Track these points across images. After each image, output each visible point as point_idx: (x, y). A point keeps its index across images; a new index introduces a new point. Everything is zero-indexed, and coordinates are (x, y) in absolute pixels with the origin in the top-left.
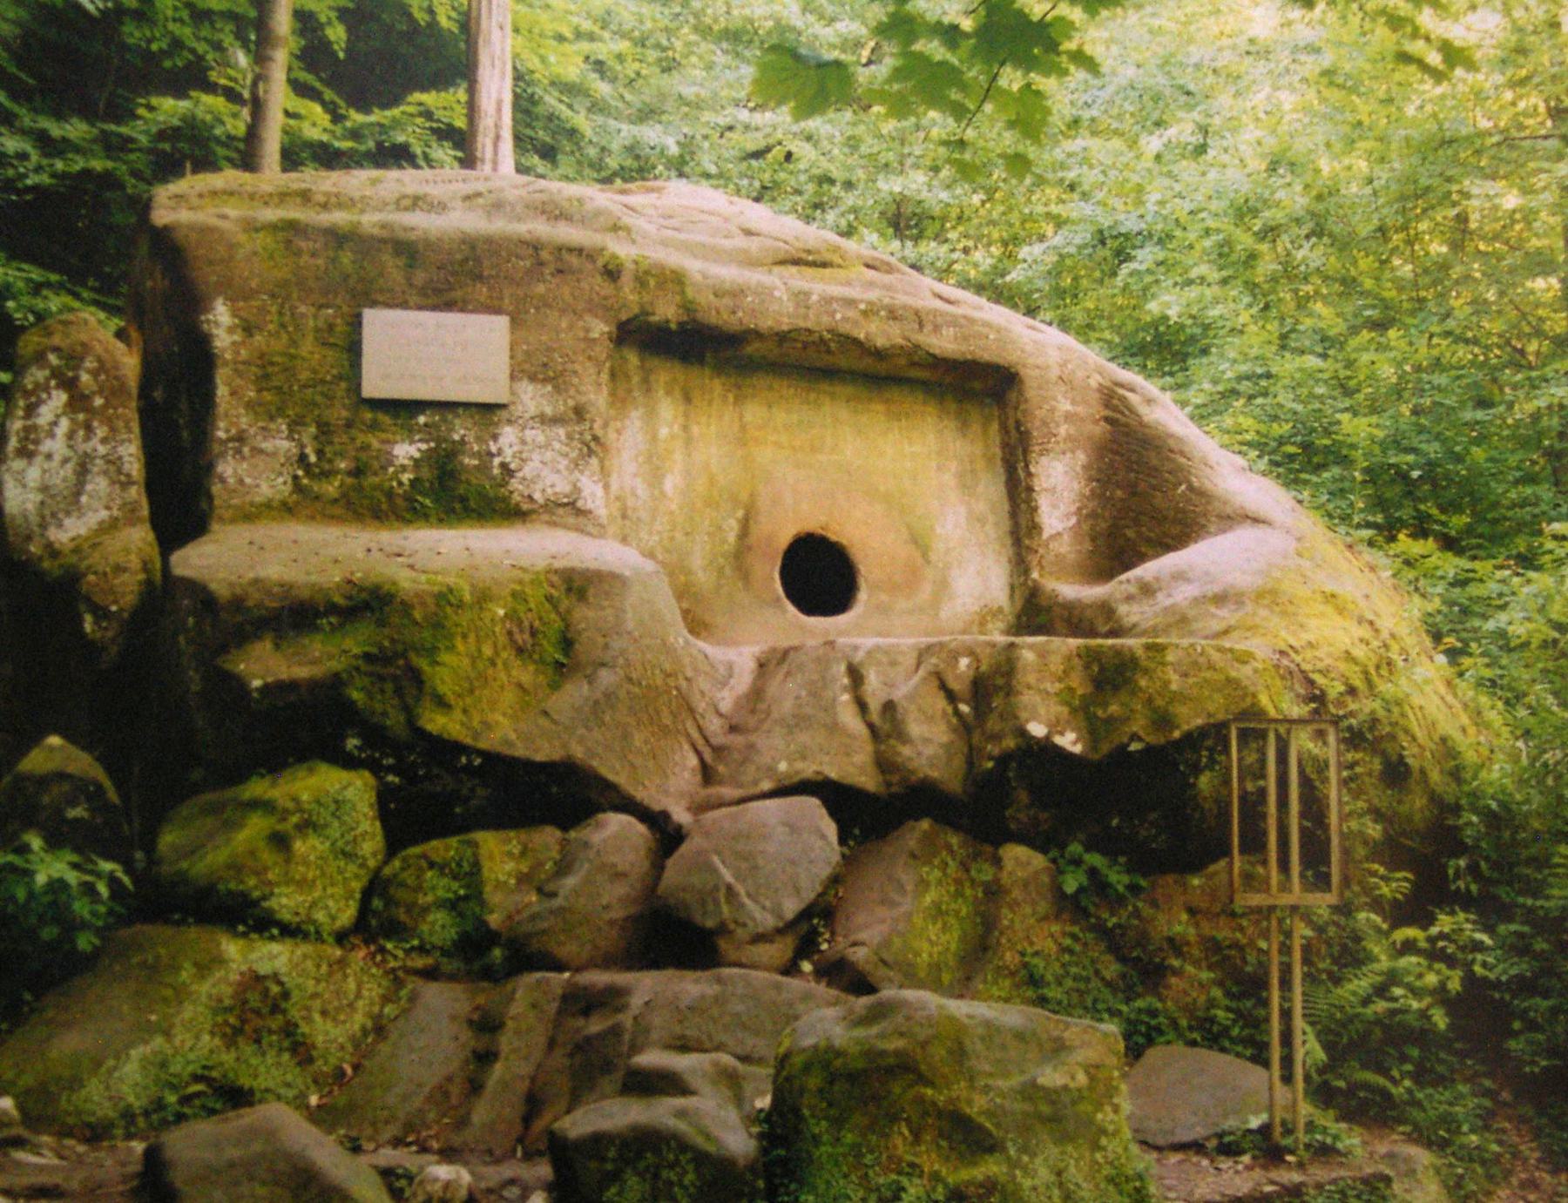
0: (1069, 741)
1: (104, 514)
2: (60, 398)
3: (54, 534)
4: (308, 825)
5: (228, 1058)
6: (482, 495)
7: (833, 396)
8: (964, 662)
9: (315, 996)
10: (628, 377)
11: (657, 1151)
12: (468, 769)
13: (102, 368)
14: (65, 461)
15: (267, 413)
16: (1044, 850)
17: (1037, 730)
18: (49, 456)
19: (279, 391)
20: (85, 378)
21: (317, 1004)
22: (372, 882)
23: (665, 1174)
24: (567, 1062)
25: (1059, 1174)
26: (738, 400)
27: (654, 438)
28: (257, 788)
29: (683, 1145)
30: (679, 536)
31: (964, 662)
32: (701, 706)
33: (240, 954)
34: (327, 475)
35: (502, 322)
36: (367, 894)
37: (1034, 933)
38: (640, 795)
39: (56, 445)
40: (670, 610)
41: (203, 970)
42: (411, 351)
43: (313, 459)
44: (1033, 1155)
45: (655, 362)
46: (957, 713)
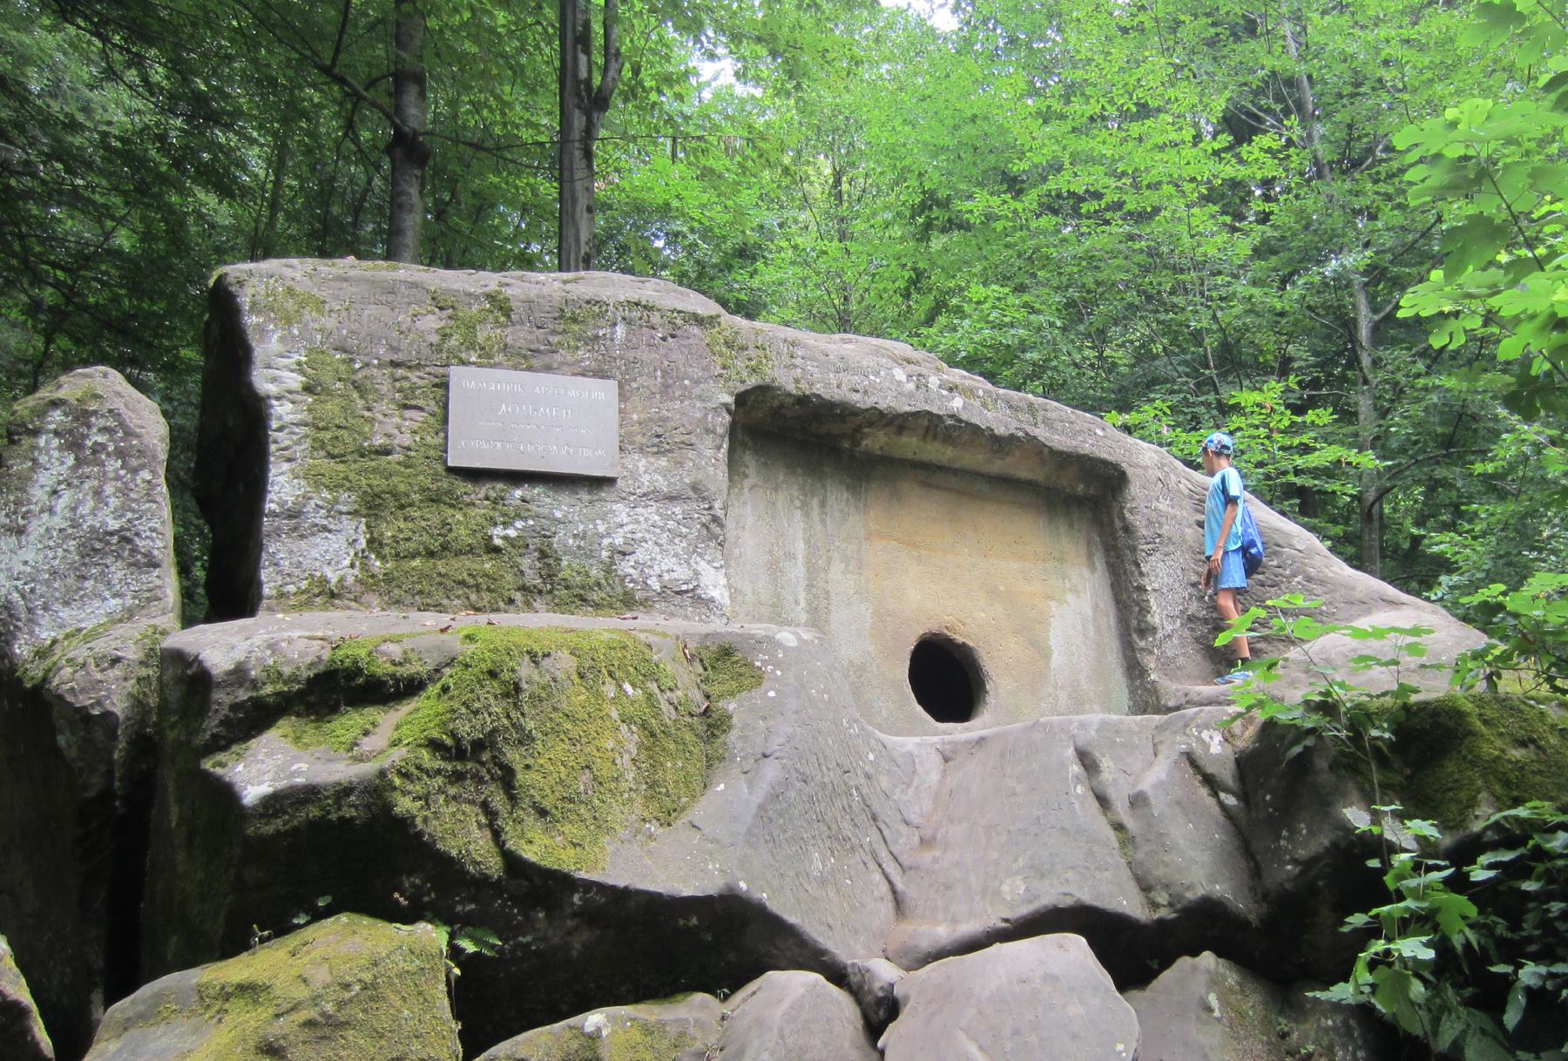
32: (886, 813)
35: (612, 386)
43: (355, 395)
46: (1221, 804)
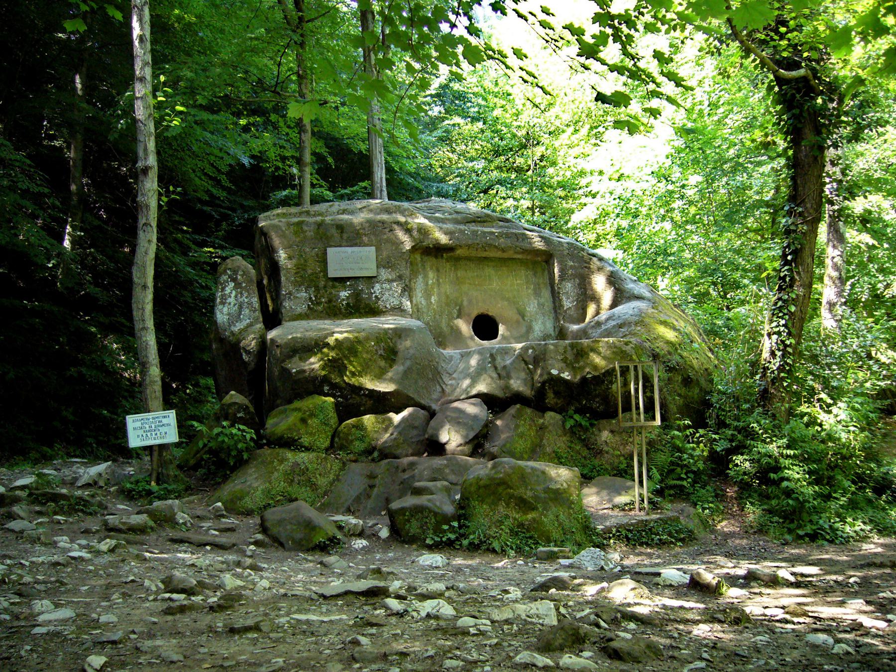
0: (566, 375)
1: (248, 321)
2: (232, 284)
3: (233, 328)
4: (313, 415)
5: (289, 489)
6: (367, 305)
7: (488, 266)
8: (530, 351)
9: (317, 469)
10: (417, 265)
11: (422, 513)
12: (364, 395)
13: (244, 273)
14: (235, 305)
15: (297, 284)
16: (560, 413)
17: (554, 372)
18: (230, 304)
19: (306, 279)
20: (239, 277)
21: (318, 472)
22: (335, 433)
23: (425, 520)
24: (398, 487)
25: (557, 517)
26: (456, 269)
27: (427, 284)
28: (297, 404)
29: (430, 511)
30: (437, 316)
31: (530, 351)
33: (291, 456)
34: (318, 304)
36: (333, 437)
37: (557, 442)
38: (423, 402)
39: (232, 300)
40: (430, 339)
41: (281, 461)
42: (344, 261)
44: (547, 511)
45: (425, 258)
46: (528, 368)
